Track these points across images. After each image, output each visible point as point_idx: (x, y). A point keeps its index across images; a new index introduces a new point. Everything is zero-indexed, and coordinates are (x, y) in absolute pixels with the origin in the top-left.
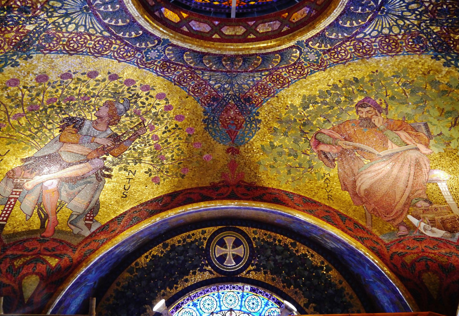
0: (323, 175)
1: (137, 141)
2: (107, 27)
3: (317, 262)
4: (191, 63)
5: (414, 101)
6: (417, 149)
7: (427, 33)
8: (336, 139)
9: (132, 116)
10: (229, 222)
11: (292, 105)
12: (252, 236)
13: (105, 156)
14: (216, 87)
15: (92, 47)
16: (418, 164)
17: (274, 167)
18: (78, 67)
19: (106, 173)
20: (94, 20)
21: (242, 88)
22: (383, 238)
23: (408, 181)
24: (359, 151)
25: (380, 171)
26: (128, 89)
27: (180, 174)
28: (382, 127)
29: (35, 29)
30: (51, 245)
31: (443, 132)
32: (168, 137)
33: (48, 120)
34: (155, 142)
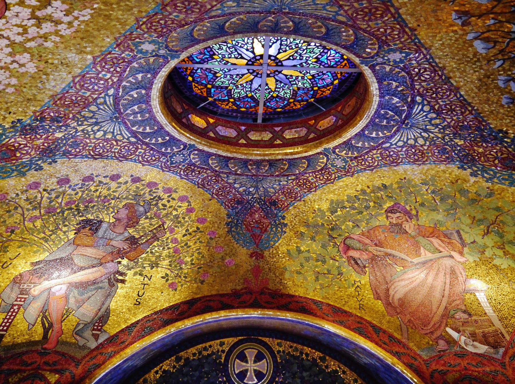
0: (353, 282)
1: (155, 244)
2: (134, 134)
3: (349, 380)
4: (216, 167)
5: (444, 208)
6: (451, 257)
7: (452, 145)
8: (366, 244)
9: (151, 218)
10: (250, 333)
11: (319, 209)
12: (276, 348)
13: (120, 260)
14: (241, 189)
15: (118, 152)
16: (453, 272)
17: (300, 273)
18: (100, 171)
19: (120, 278)
20: (123, 128)
21: (268, 192)
22: (421, 353)
23: (444, 290)
24: (391, 257)
25: (413, 279)
26: (150, 191)
27: (200, 280)
28: (413, 234)
29: (64, 136)
30: (52, 358)
32: (189, 240)
33: (64, 222)
34: (174, 245)
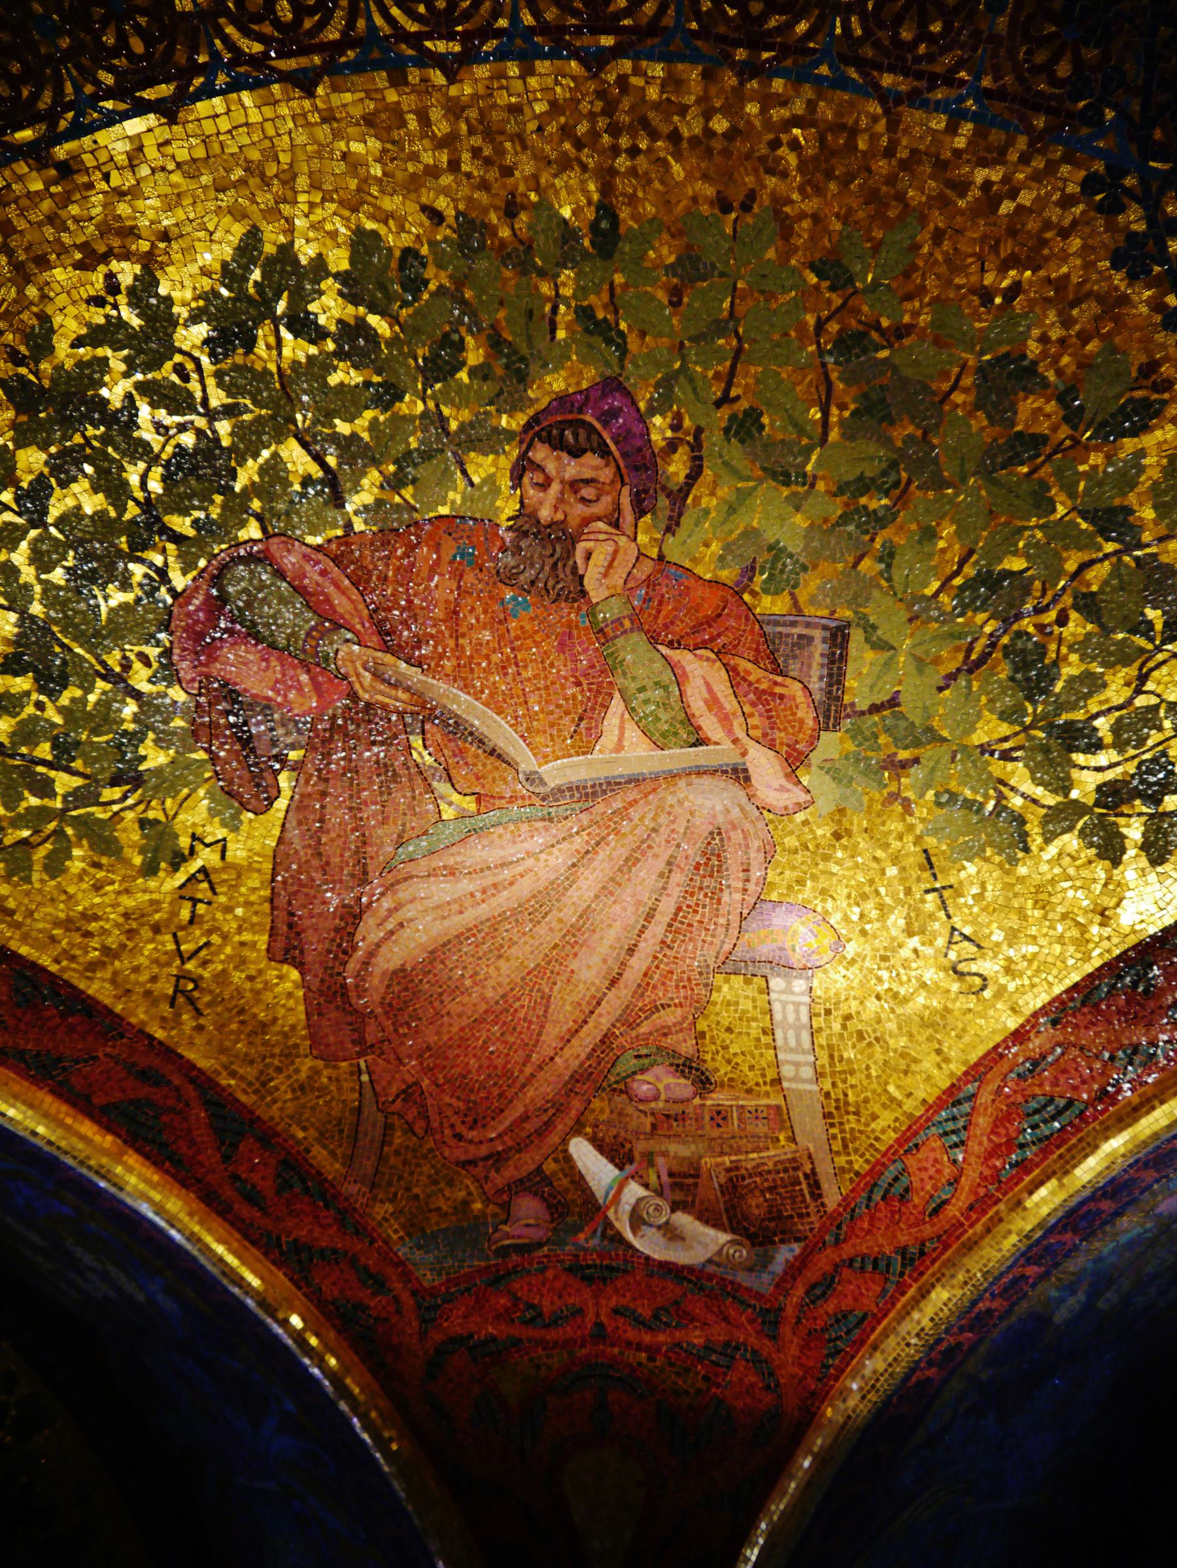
0: (184, 842)
6: (740, 775)
22: (418, 1255)
23: (631, 951)
25: (506, 873)
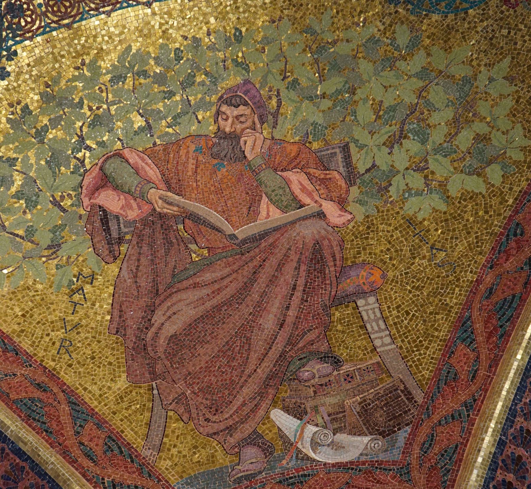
6: (321, 215)
31: (377, 163)
